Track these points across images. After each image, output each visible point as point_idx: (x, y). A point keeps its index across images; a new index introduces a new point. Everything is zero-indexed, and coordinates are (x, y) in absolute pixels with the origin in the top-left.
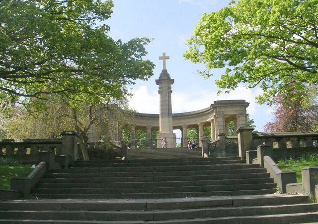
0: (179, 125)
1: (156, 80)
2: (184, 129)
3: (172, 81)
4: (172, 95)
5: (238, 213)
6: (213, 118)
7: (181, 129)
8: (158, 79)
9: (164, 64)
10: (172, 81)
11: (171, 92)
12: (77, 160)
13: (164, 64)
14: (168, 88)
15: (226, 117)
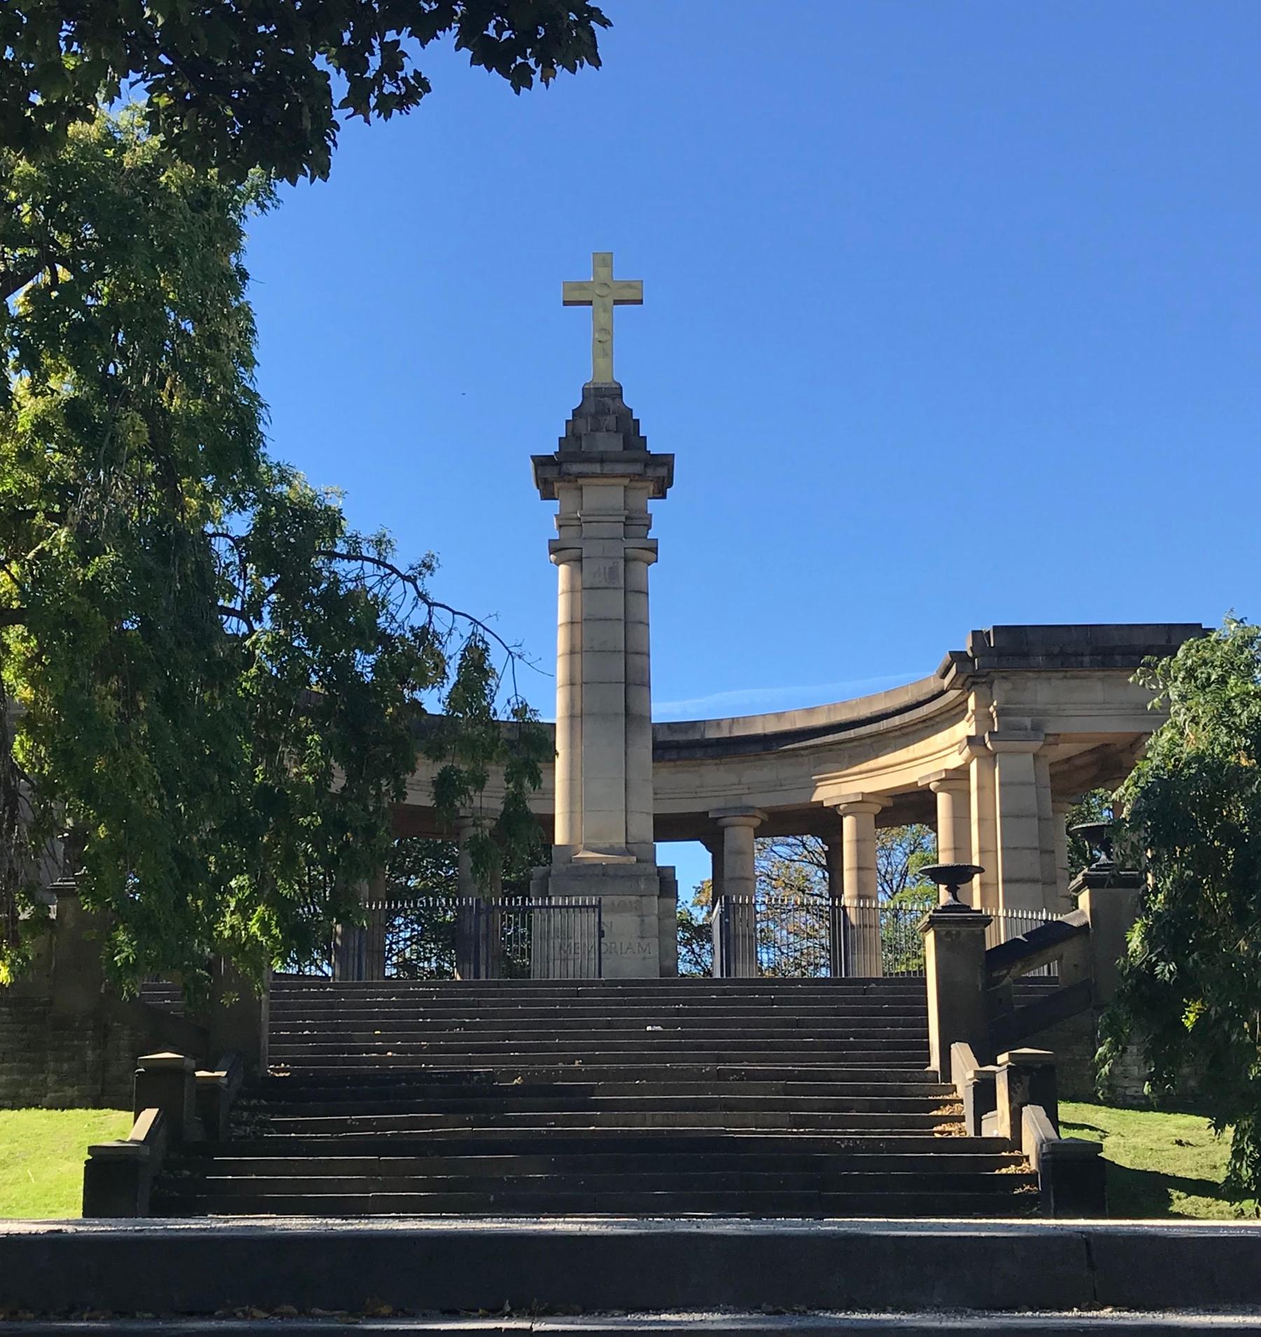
0: (696, 807)
1: (541, 463)
2: (738, 834)
3: (658, 473)
4: (656, 576)
5: (345, 1062)
6: (955, 761)
7: (715, 844)
8: (551, 449)
9: (604, 345)
10: (658, 473)
11: (670, 485)
12: (1227, 1128)
13: (604, 345)
14: (628, 522)
15: (1065, 750)
